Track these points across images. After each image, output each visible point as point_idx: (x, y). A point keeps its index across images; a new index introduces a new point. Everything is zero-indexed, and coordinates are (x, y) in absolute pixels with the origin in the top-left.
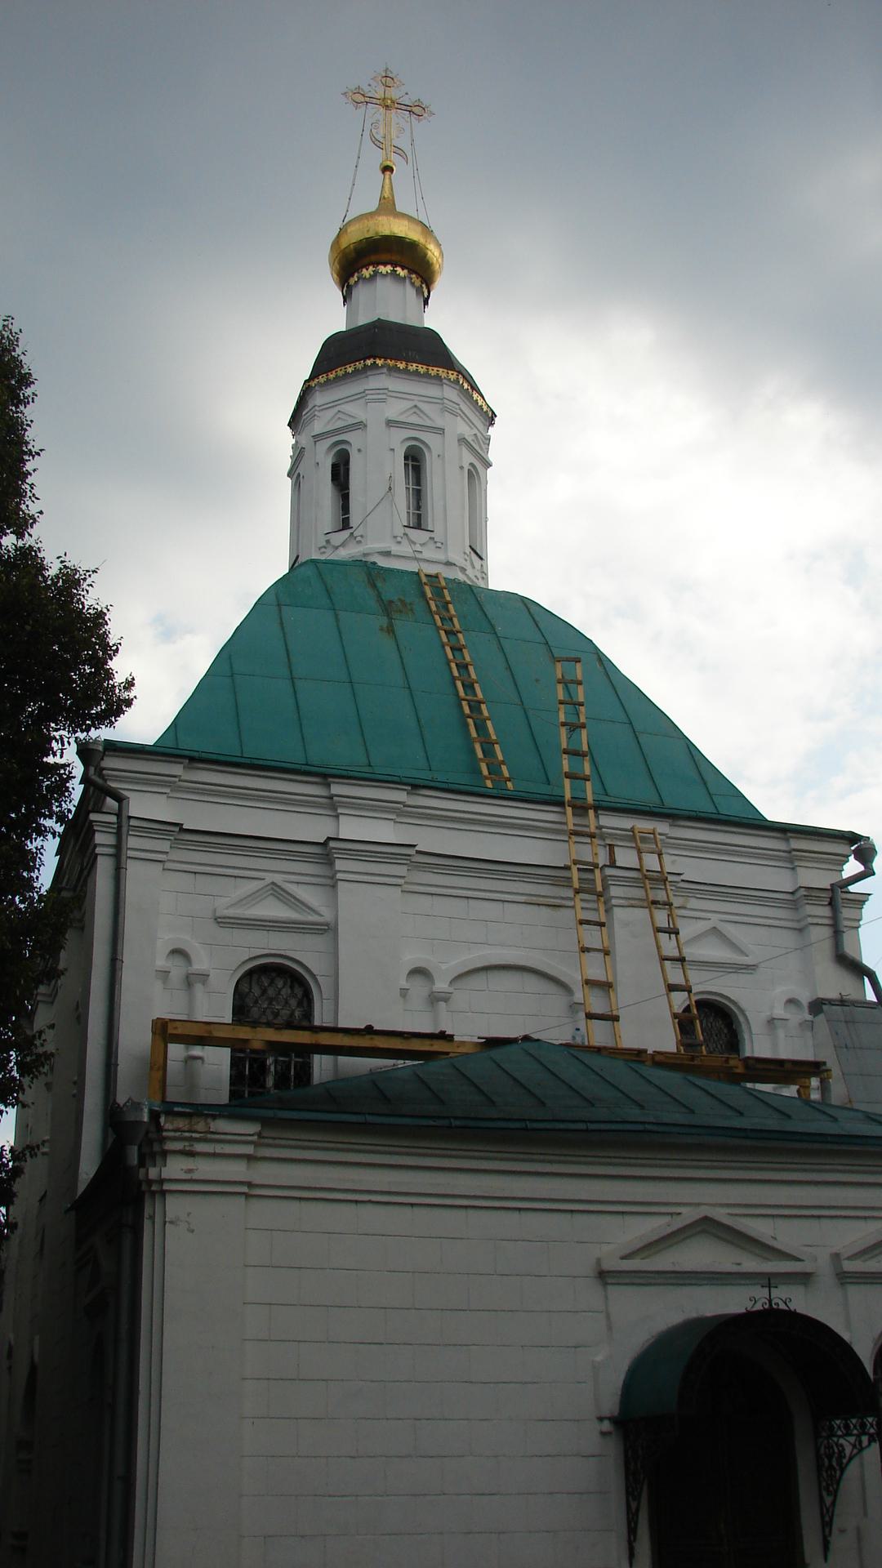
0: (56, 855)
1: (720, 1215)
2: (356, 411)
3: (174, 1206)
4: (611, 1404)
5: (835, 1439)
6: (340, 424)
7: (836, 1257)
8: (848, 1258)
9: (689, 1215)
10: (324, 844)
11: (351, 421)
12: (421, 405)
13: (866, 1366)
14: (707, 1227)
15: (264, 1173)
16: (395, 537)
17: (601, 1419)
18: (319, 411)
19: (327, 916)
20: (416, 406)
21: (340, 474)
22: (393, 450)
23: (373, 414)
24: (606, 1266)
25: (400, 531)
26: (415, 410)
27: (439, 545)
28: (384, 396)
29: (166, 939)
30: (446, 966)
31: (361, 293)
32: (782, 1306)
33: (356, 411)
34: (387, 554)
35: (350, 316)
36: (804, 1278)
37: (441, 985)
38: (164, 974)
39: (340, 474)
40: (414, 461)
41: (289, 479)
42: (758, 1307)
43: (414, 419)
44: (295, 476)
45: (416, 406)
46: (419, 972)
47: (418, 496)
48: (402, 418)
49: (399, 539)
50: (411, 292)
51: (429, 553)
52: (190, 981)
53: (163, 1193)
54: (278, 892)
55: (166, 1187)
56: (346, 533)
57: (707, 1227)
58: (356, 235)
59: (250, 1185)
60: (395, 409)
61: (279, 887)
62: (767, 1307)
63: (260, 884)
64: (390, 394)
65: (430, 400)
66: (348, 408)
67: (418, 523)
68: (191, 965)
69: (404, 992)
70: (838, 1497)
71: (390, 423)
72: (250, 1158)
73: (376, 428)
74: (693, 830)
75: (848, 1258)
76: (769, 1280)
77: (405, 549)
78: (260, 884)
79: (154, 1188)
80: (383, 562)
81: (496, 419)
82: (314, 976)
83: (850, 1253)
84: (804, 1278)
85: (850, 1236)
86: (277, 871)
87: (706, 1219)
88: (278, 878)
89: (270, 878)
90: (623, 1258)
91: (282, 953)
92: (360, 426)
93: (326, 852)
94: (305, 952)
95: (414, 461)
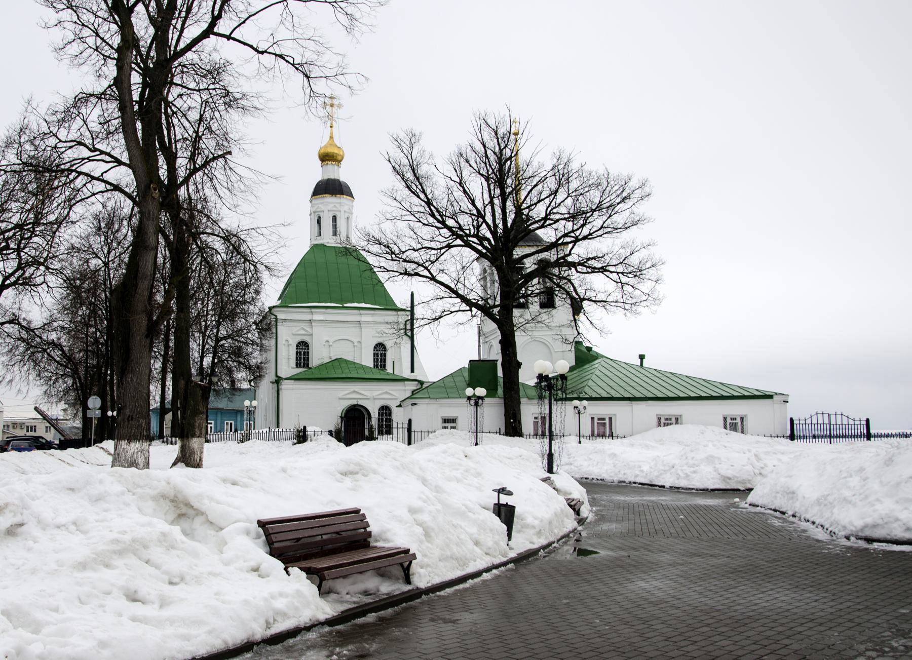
0: (279, 300)
1: (356, 390)
3: (283, 391)
9: (352, 390)
14: (355, 392)
21: (319, 222)
29: (285, 338)
30: (331, 341)
33: (322, 207)
34: (328, 243)
35: (323, 176)
37: (331, 344)
38: (284, 345)
39: (319, 222)
43: (335, 209)
46: (327, 341)
52: (289, 345)
54: (303, 329)
56: (320, 237)
57: (355, 392)
58: (322, 151)
60: (330, 207)
66: (320, 205)
69: (324, 345)
70: (592, 274)
73: (326, 212)
74: (276, 396)
77: (332, 241)
80: (327, 245)
86: (303, 325)
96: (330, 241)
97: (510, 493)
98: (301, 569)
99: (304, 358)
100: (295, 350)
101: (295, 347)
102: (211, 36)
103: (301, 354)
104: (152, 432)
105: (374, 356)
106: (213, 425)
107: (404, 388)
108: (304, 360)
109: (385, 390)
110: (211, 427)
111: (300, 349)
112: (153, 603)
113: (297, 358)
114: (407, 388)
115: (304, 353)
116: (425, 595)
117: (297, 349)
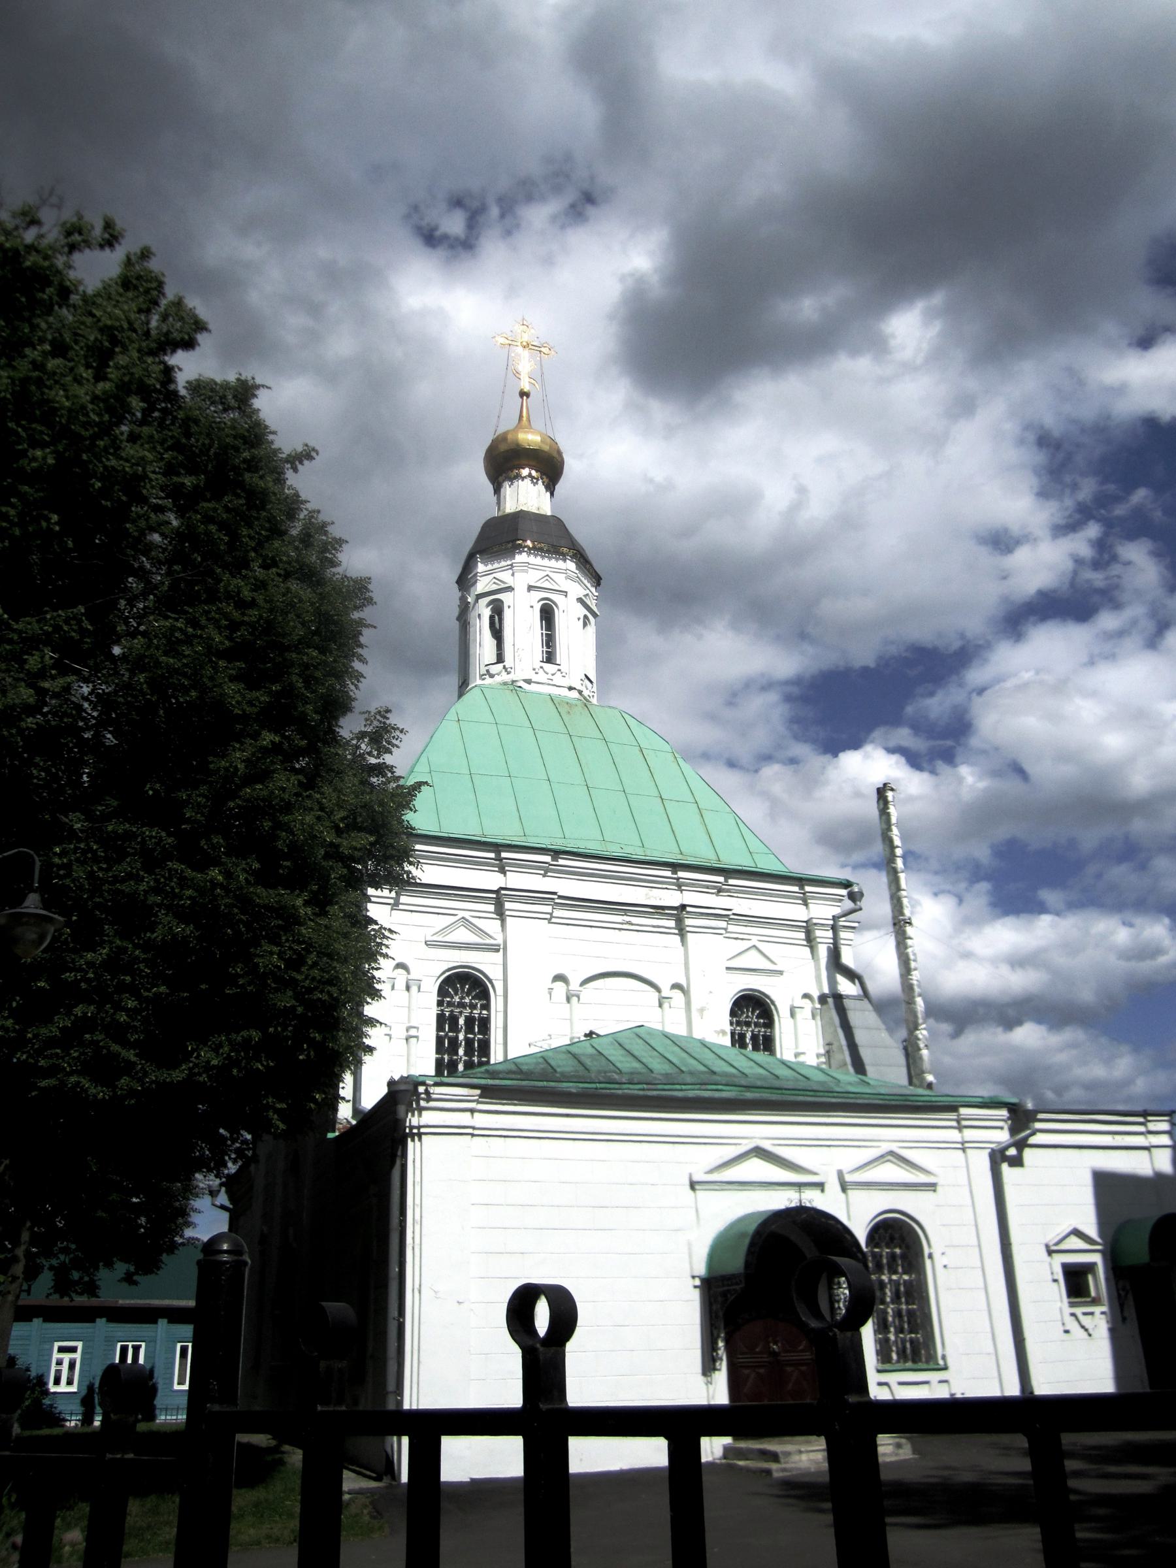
1: (767, 1145)
2: (505, 576)
4: (701, 1269)
5: (841, 1290)
6: (495, 587)
7: (840, 1174)
8: (849, 1172)
9: (747, 1146)
10: (497, 892)
11: (503, 586)
12: (551, 575)
13: (825, 1316)
14: (760, 1152)
15: (480, 1120)
16: (534, 669)
17: (693, 1277)
18: (480, 577)
19: (500, 941)
20: (547, 575)
22: (532, 607)
23: (520, 581)
24: (696, 1178)
25: (538, 664)
26: (547, 578)
27: (564, 674)
28: (526, 568)
31: (508, 490)
32: (808, 1205)
33: (505, 576)
36: (821, 1186)
40: (547, 615)
41: (458, 622)
42: (793, 1205)
44: (462, 621)
45: (547, 575)
46: (560, 978)
47: (549, 641)
48: (538, 584)
49: (537, 671)
50: (540, 486)
51: (558, 679)
53: (420, 1135)
55: (422, 1130)
56: (500, 666)
57: (760, 1152)
59: (474, 1128)
60: (533, 577)
61: (467, 920)
62: (798, 1204)
63: (454, 919)
64: (530, 566)
65: (558, 571)
66: (499, 575)
67: (550, 658)
68: (409, 973)
71: (530, 588)
72: (472, 1111)
75: (849, 1172)
76: (800, 1186)
77: (542, 677)
78: (454, 919)
79: (415, 1131)
81: (602, 581)
82: (490, 981)
83: (850, 1169)
84: (821, 1186)
85: (848, 1159)
87: (891, 1153)
88: (467, 915)
89: (461, 914)
90: (706, 1173)
91: (474, 965)
92: (510, 589)
93: (498, 899)
94: (487, 964)
95: (547, 615)
96: (535, 678)
97: (317, 454)
98: (891, 751)
99: (469, 1043)
100: (434, 1011)
101: (434, 998)
102: (257, 392)
103: (454, 1027)
104: (564, 1063)
105: (440, 1027)
106: (77, 1356)
107: (954, 1135)
108: (469, 1051)
109: (885, 1147)
110: (72, 1365)
111: (450, 1004)
112: (927, 859)
113: (439, 1041)
114: (969, 1134)
115: (470, 1021)
116: (916, 1029)
117: (440, 1004)
